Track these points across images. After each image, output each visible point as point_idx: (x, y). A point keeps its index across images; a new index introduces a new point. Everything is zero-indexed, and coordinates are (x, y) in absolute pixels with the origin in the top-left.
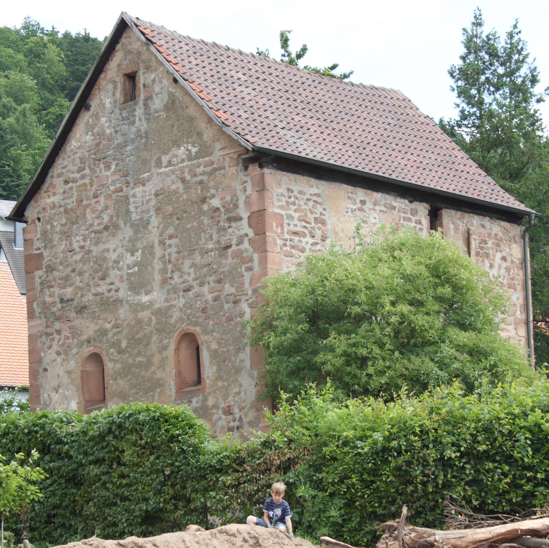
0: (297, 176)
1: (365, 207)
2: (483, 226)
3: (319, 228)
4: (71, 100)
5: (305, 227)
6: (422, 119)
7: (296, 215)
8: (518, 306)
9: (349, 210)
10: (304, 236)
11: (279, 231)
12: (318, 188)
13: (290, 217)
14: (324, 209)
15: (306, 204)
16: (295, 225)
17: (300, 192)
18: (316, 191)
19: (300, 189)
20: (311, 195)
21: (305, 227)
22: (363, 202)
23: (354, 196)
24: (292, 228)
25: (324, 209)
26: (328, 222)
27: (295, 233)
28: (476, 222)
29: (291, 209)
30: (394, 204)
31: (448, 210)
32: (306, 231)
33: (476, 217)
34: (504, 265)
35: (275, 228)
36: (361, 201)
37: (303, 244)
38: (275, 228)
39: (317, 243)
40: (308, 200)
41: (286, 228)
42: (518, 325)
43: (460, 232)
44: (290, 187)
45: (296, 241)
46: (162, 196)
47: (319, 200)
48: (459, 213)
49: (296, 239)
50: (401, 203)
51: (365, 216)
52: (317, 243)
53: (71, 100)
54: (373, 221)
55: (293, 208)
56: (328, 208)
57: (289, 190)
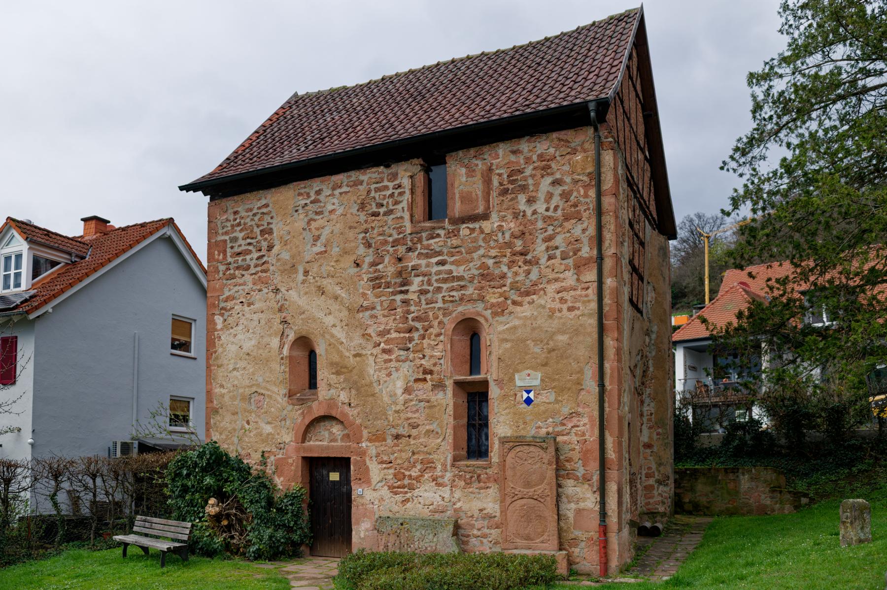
0: (242, 196)
1: (321, 197)
3: (266, 239)
5: (250, 244)
6: (512, 53)
7: (241, 235)
8: (585, 241)
9: (300, 208)
13: (235, 239)
15: (252, 220)
18: (264, 202)
19: (247, 207)
20: (259, 208)
23: (307, 190)
24: (236, 250)
26: (275, 230)
27: (239, 254)
28: (501, 156)
31: (454, 154)
33: (501, 145)
34: (558, 190)
37: (248, 262)
42: (582, 268)
43: (479, 174)
46: (880, 542)
47: (265, 210)
48: (472, 151)
50: (368, 176)
51: (320, 207)
52: (264, 256)
54: (330, 207)
55: (238, 229)
57: (236, 213)
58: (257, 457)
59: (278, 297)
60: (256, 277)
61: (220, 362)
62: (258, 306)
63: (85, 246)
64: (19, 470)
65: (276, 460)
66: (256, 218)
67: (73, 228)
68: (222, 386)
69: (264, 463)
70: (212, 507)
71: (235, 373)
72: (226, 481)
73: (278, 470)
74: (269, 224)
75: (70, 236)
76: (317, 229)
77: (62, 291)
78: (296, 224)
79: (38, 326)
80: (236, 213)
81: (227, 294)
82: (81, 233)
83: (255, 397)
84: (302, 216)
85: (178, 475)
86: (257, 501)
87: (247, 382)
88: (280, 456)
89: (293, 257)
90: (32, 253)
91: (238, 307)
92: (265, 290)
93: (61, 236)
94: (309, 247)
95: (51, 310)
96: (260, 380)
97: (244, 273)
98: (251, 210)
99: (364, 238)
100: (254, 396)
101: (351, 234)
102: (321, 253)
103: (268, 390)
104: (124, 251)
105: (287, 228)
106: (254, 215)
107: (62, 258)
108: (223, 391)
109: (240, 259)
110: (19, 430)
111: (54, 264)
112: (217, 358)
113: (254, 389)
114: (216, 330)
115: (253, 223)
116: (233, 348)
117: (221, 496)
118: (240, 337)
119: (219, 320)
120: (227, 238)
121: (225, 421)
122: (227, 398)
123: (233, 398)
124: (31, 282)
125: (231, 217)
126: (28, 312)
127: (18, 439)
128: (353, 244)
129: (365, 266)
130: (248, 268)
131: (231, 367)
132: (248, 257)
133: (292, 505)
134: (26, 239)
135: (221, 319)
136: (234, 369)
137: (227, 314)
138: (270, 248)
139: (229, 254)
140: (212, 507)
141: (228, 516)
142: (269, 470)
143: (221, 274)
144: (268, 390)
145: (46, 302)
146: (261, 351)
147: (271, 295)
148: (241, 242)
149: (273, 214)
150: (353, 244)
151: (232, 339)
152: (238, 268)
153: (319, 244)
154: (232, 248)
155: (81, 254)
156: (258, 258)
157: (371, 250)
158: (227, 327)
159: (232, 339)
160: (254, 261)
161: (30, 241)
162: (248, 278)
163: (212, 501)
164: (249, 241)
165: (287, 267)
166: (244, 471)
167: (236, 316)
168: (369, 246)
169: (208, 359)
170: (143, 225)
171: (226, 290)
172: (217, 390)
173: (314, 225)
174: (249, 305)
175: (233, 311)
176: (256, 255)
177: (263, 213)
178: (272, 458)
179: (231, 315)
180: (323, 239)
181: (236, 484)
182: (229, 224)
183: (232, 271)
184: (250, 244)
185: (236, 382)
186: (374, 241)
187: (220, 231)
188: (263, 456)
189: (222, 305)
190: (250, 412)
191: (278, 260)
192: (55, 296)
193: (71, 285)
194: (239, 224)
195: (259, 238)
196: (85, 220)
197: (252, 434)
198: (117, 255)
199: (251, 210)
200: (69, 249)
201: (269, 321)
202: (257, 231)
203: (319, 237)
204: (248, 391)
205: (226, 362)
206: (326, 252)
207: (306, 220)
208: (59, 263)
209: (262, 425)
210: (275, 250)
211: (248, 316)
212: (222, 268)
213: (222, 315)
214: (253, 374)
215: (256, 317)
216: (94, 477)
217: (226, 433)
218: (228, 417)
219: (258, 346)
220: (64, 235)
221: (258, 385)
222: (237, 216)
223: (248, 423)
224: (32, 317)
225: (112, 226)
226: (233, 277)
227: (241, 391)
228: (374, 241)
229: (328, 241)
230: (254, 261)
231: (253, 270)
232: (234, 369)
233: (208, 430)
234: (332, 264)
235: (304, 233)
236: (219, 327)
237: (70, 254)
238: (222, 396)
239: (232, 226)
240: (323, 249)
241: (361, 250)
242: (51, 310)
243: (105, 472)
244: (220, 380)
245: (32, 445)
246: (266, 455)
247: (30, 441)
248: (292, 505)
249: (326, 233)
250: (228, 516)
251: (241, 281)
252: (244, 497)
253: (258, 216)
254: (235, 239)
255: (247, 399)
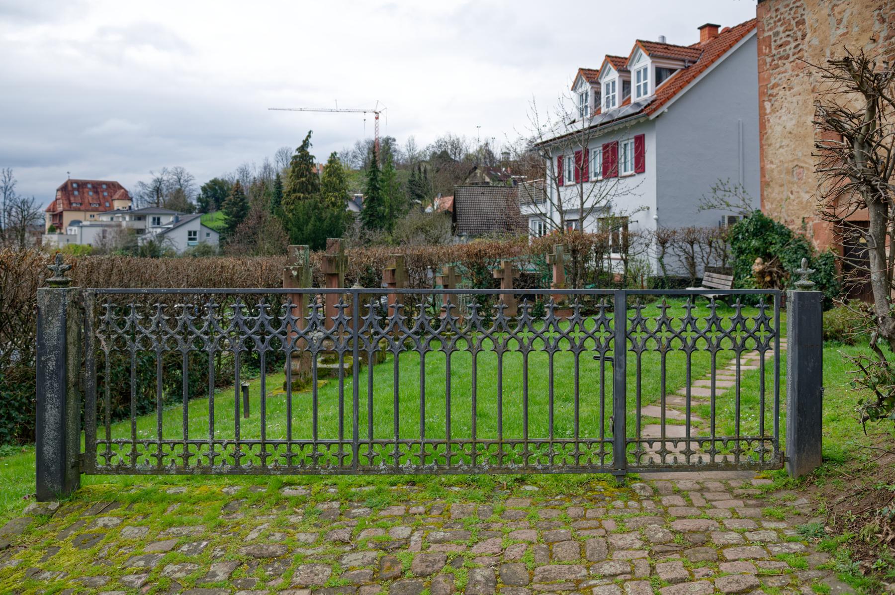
3: (800, 30)
5: (788, 36)
7: (781, 29)
13: (777, 34)
24: (779, 42)
27: (781, 46)
55: (779, 24)
58: (799, 222)
59: (811, 79)
60: (794, 64)
61: (769, 142)
62: (796, 89)
63: (699, 52)
64: (635, 238)
65: (814, 225)
66: (792, 12)
67: (689, 37)
68: (772, 162)
69: (804, 228)
70: (757, 265)
71: (781, 150)
72: (771, 244)
73: (815, 234)
74: (802, 15)
75: (687, 45)
76: (840, 13)
77: (675, 93)
78: (823, 12)
79: (658, 124)
80: (777, 10)
81: (773, 82)
82: (698, 40)
83: (797, 170)
84: (827, 4)
85: (736, 239)
86: (794, 261)
87: (790, 157)
88: (817, 221)
89: (821, 42)
90: (654, 65)
91: (781, 93)
92: (801, 75)
93: (684, 48)
94: (833, 31)
95: (666, 110)
96: (800, 154)
97: (785, 61)
98: (788, 5)
99: (878, 14)
100: (795, 169)
101: (867, 13)
102: (844, 34)
103: (806, 163)
104: (725, 51)
105: (815, 17)
106: (791, 9)
107: (678, 65)
108: (774, 166)
109: (782, 50)
110: (648, 209)
111: (672, 71)
112: (767, 139)
113: (795, 163)
114: (766, 114)
115: (790, 17)
116: (778, 129)
117: (767, 256)
118: (784, 118)
119: (767, 105)
120: (771, 33)
121: (774, 193)
122: (775, 173)
123: (780, 172)
124: (655, 89)
125: (774, 15)
126: (648, 114)
127: (648, 216)
128: (869, 22)
129: (881, 41)
130: (787, 57)
131: (778, 145)
132: (787, 48)
133: (825, 264)
134: (649, 55)
135: (770, 104)
136: (781, 147)
137: (773, 99)
138: (804, 36)
139: (773, 47)
140: (757, 265)
141: (771, 273)
142: (809, 233)
143: (768, 66)
144: (806, 163)
145: (662, 104)
146: (800, 129)
147: (806, 78)
148: (782, 35)
149: (805, 6)
150: (869, 22)
151: (778, 121)
152: (780, 58)
153: (841, 26)
154: (775, 41)
155: (693, 59)
156: (795, 47)
157: (886, 24)
158: (774, 111)
159: (778, 121)
160: (792, 50)
161: (652, 56)
162: (788, 66)
163: (758, 260)
164: (788, 33)
165: (817, 52)
166: (785, 235)
167: (780, 101)
168: (883, 21)
169: (761, 140)
170: (743, 25)
171: (772, 78)
172: (768, 166)
173: (837, 10)
174: (790, 89)
175: (778, 97)
176: (793, 45)
177: (797, 7)
178: (811, 223)
179: (776, 101)
180: (845, 21)
181: (778, 246)
182: (772, 21)
183: (776, 62)
184: (788, 36)
185: (782, 158)
186: (887, 16)
187: (766, 29)
188: (803, 221)
189: (770, 92)
190: (793, 183)
191: (810, 46)
192: (668, 99)
193: (681, 87)
194: (779, 20)
195: (795, 29)
196: (701, 28)
197: (795, 203)
198: (719, 56)
199: (788, 5)
200: (683, 57)
201: (805, 101)
202: (793, 23)
203: (841, 20)
204: (791, 165)
205: (774, 141)
206: (847, 33)
207: (830, 6)
208: (675, 70)
209: (803, 194)
210: (807, 38)
211: (789, 99)
212: (769, 60)
213: (770, 101)
214: (795, 150)
215: (795, 99)
216: (692, 243)
217: (776, 203)
218: (777, 189)
219: (798, 125)
220: (681, 45)
221: (798, 159)
222: (778, 13)
223: (792, 193)
224: (652, 117)
225: (728, 30)
226: (777, 66)
227: (786, 165)
228: (887, 16)
229: (849, 22)
230: (792, 50)
231: (791, 59)
232: (781, 147)
233: (762, 201)
234: (853, 43)
235: (829, 18)
236: (768, 111)
237: (684, 61)
238: (772, 171)
239: (775, 22)
240: (845, 31)
241: (877, 26)
242: (666, 110)
243: (701, 240)
244: (770, 157)
245: (657, 220)
246: (806, 221)
247: (655, 216)
248: (825, 264)
249: (846, 15)
250: (771, 273)
251: (782, 69)
252: (783, 258)
253: (794, 10)
254: (777, 34)
255: (790, 172)
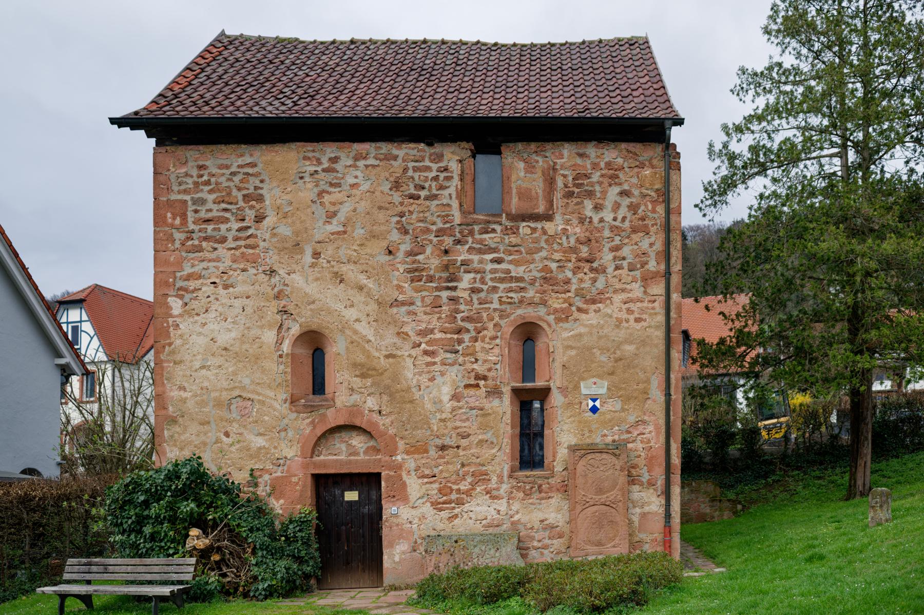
1: (339, 166)
2: (581, 155)
4: (519, 188)
5: (226, 210)
10: (227, 220)
11: (178, 221)
12: (251, 155)
14: (262, 181)
16: (211, 210)
17: (221, 167)
18: (248, 159)
21: (226, 210)
22: (334, 160)
23: (317, 155)
25: (262, 181)
26: (267, 197)
29: (202, 190)
30: (395, 152)
32: (227, 215)
33: (566, 145)
34: (626, 201)
35: (170, 221)
36: (330, 159)
38: (170, 221)
39: (249, 227)
40: (233, 174)
41: (191, 216)
44: (201, 163)
45: (209, 231)
48: (533, 146)
49: (210, 227)
51: (336, 178)
52: (249, 227)
53: (519, 188)
55: (207, 188)
56: (267, 179)
